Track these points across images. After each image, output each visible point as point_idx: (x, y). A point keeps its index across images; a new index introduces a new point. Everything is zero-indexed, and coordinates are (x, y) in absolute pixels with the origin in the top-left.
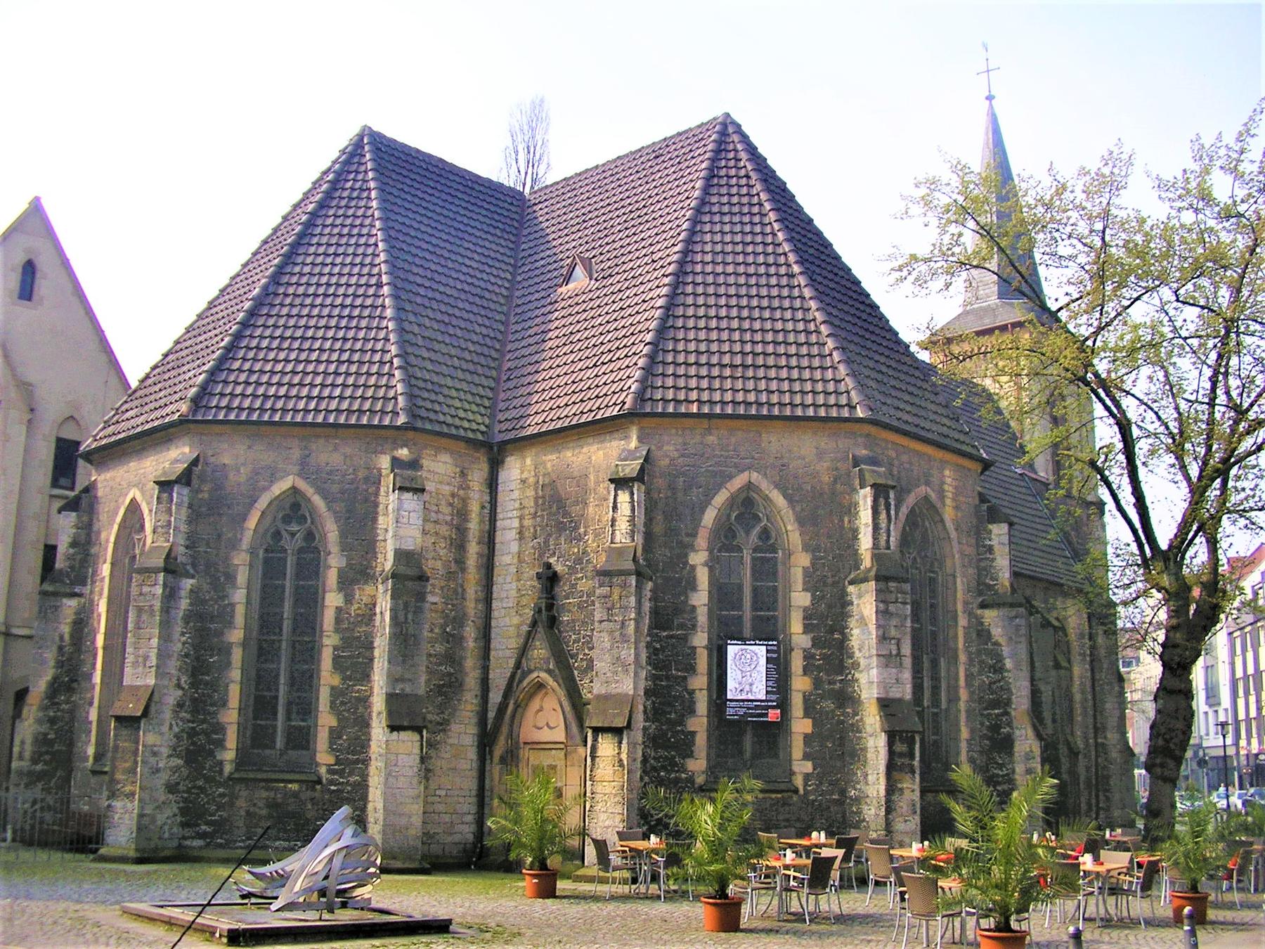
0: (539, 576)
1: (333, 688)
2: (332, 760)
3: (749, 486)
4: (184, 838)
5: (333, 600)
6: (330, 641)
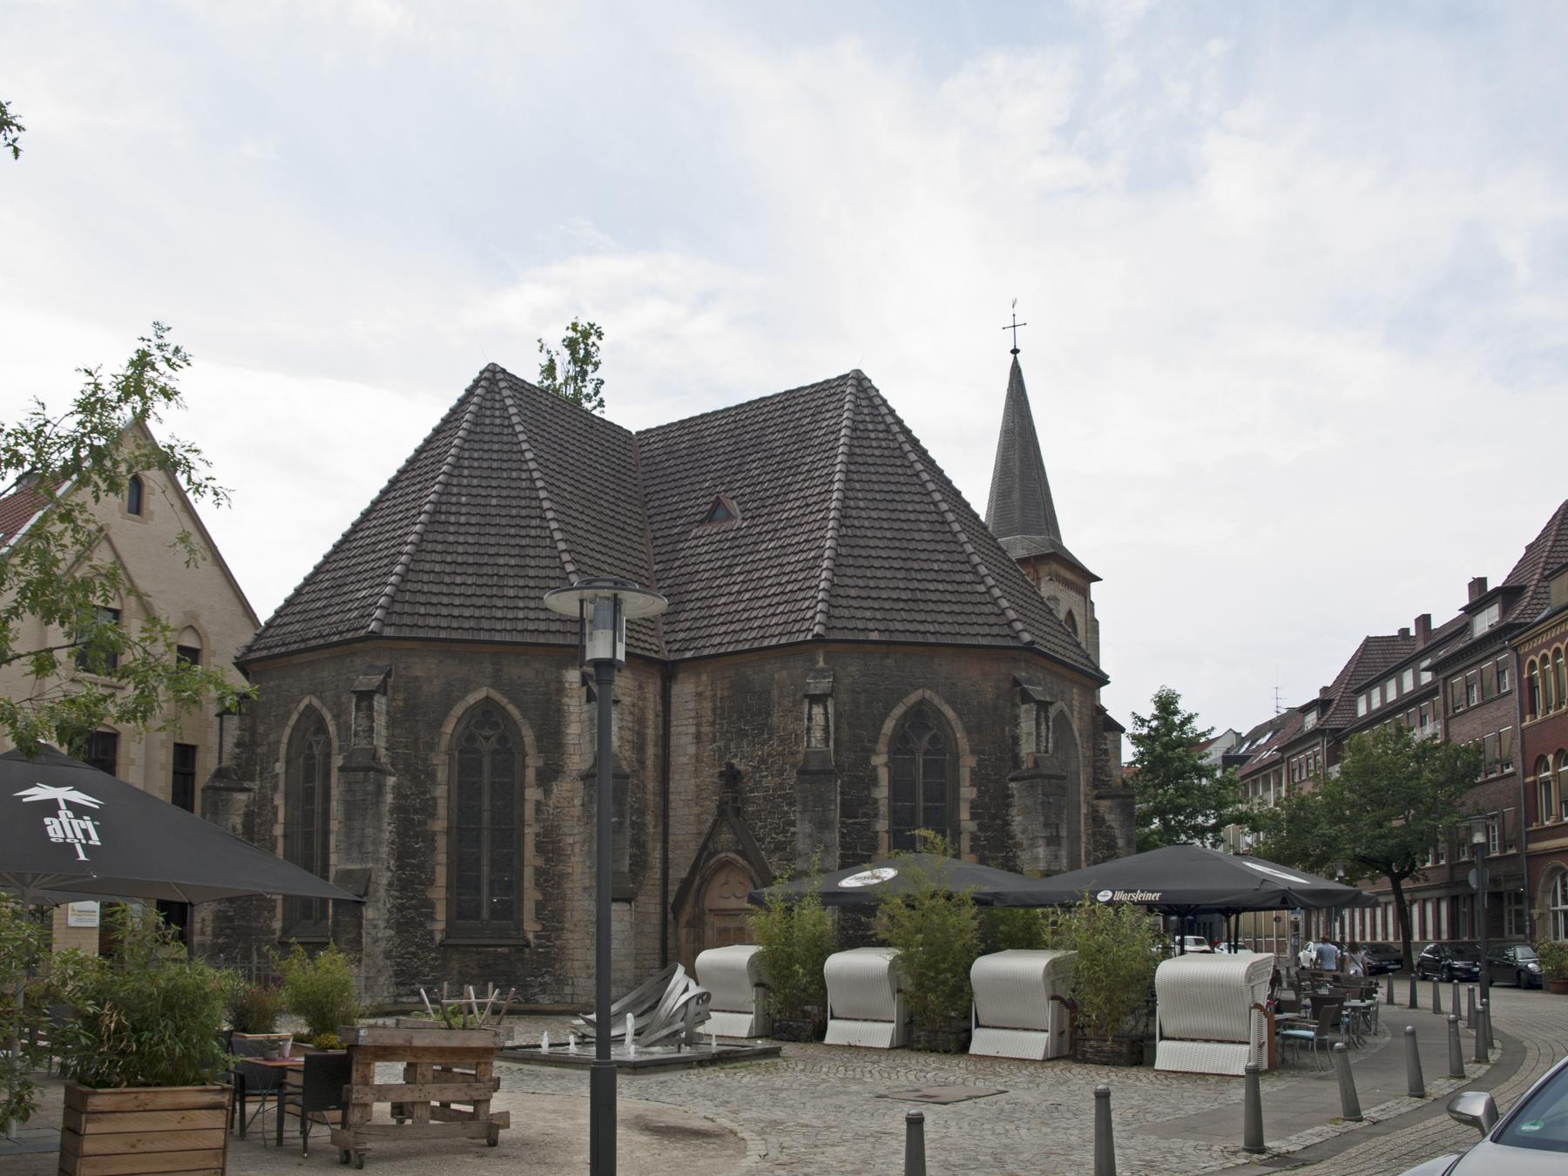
0: (722, 774)
1: (536, 868)
2: (538, 927)
3: (923, 701)
4: (400, 995)
5: (532, 794)
6: (530, 832)
